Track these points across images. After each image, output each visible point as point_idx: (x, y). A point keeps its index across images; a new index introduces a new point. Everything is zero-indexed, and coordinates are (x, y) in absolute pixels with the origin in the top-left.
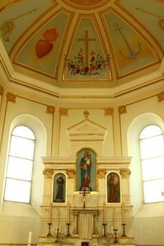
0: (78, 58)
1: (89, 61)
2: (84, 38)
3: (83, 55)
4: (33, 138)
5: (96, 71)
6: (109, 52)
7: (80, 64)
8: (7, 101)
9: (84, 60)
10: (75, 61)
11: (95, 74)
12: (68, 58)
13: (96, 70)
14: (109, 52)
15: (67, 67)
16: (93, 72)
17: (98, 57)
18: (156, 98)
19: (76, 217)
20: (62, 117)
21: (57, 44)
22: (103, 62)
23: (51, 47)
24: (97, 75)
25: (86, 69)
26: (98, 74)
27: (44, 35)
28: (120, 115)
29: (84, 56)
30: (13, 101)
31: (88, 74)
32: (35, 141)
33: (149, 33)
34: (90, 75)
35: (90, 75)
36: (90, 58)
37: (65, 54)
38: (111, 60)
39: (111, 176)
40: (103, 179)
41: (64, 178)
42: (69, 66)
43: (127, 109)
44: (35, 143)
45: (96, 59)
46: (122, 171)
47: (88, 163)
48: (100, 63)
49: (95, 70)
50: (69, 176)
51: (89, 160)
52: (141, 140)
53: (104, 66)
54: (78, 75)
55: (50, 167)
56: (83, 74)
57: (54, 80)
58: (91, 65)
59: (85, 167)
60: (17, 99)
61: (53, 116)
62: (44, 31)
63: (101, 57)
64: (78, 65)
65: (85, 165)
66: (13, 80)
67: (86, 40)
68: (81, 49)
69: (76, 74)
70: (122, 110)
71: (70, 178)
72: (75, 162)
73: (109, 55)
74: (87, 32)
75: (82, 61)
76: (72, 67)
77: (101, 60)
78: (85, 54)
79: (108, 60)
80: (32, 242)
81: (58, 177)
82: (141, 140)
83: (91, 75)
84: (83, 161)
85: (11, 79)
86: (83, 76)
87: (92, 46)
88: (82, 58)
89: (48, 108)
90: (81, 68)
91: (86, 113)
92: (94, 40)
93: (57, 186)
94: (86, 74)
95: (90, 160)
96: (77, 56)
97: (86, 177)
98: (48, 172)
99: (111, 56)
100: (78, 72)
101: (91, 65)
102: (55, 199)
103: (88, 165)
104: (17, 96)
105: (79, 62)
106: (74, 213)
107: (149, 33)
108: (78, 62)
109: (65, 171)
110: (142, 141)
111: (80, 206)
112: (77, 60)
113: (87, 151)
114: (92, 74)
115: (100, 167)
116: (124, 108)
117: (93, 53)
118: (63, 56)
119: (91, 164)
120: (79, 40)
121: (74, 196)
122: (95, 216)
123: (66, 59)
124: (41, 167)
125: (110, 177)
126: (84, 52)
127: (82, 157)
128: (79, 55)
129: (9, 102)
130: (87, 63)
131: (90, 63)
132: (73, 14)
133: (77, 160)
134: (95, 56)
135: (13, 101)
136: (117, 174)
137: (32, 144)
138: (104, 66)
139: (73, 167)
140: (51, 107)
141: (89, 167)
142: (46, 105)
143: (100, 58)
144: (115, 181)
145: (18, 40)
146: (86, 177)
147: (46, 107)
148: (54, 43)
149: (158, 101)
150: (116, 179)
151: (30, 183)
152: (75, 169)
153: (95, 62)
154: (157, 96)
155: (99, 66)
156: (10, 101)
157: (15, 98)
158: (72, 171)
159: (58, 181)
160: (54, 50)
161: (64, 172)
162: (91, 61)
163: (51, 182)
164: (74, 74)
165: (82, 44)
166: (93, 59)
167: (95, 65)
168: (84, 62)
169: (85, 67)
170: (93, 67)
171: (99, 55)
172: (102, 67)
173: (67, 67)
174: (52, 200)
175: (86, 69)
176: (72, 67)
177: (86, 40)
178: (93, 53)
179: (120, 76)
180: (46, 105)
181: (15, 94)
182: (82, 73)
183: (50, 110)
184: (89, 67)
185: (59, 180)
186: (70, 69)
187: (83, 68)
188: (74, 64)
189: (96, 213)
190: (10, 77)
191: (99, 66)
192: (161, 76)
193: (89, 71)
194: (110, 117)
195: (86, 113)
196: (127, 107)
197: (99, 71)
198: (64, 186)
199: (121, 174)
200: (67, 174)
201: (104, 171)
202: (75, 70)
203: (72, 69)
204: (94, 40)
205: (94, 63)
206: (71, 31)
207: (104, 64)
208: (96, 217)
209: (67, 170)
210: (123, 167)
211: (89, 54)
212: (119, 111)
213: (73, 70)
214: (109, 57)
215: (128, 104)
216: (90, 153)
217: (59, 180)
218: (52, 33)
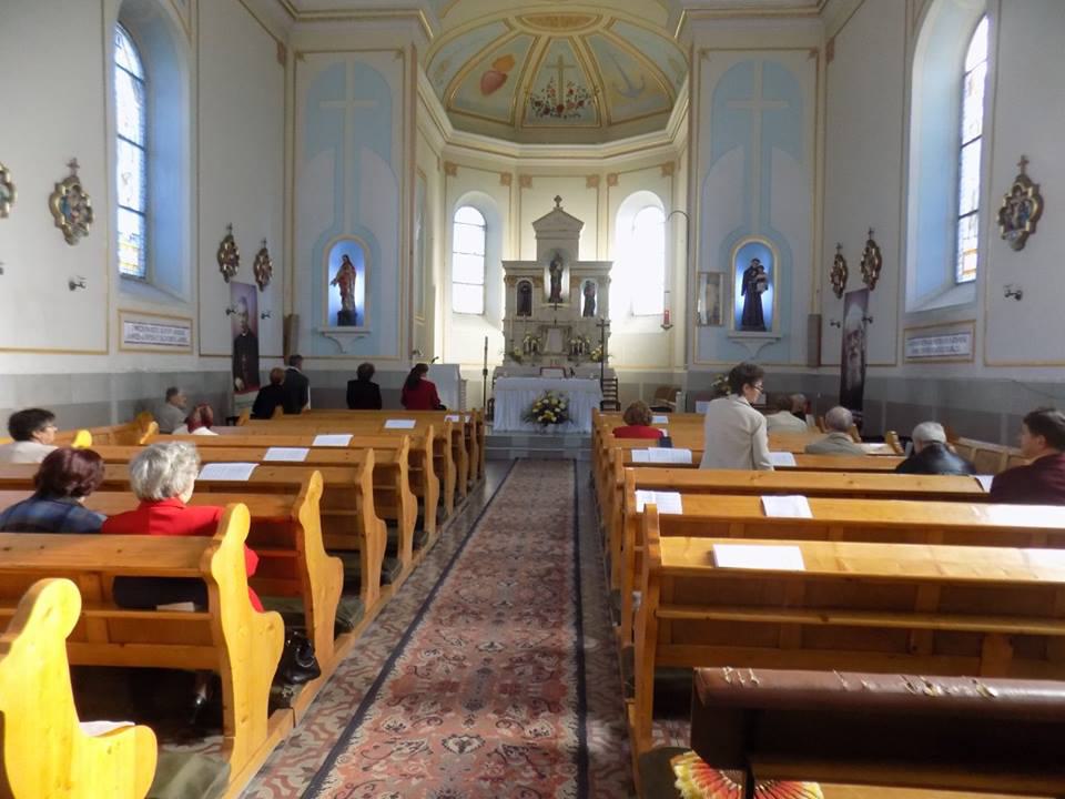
1: (564, 95)
4: (482, 223)
9: (557, 93)
20: (523, 190)
22: (587, 96)
23: (504, 78)
27: (494, 65)
29: (557, 88)
32: (486, 227)
36: (566, 91)
38: (600, 94)
43: (619, 180)
45: (575, 93)
62: (494, 60)
63: (584, 90)
70: (613, 179)
74: (561, 59)
75: (554, 95)
80: (91, 617)
88: (553, 91)
90: (551, 106)
92: (572, 67)
100: (547, 111)
104: (458, 165)
111: (549, 320)
117: (570, 84)
118: (523, 87)
121: (543, 308)
128: (549, 86)
130: (561, 97)
131: (565, 99)
132: (537, 38)
137: (481, 234)
147: (499, 176)
148: (510, 74)
152: (457, 702)
153: (573, 97)
160: (508, 80)
166: (571, 92)
167: (573, 101)
177: (561, 66)
183: (506, 178)
184: (565, 104)
189: (568, 330)
194: (594, 190)
202: (542, 110)
203: (537, 108)
204: (572, 67)
206: (536, 55)
211: (565, 84)
212: (608, 180)
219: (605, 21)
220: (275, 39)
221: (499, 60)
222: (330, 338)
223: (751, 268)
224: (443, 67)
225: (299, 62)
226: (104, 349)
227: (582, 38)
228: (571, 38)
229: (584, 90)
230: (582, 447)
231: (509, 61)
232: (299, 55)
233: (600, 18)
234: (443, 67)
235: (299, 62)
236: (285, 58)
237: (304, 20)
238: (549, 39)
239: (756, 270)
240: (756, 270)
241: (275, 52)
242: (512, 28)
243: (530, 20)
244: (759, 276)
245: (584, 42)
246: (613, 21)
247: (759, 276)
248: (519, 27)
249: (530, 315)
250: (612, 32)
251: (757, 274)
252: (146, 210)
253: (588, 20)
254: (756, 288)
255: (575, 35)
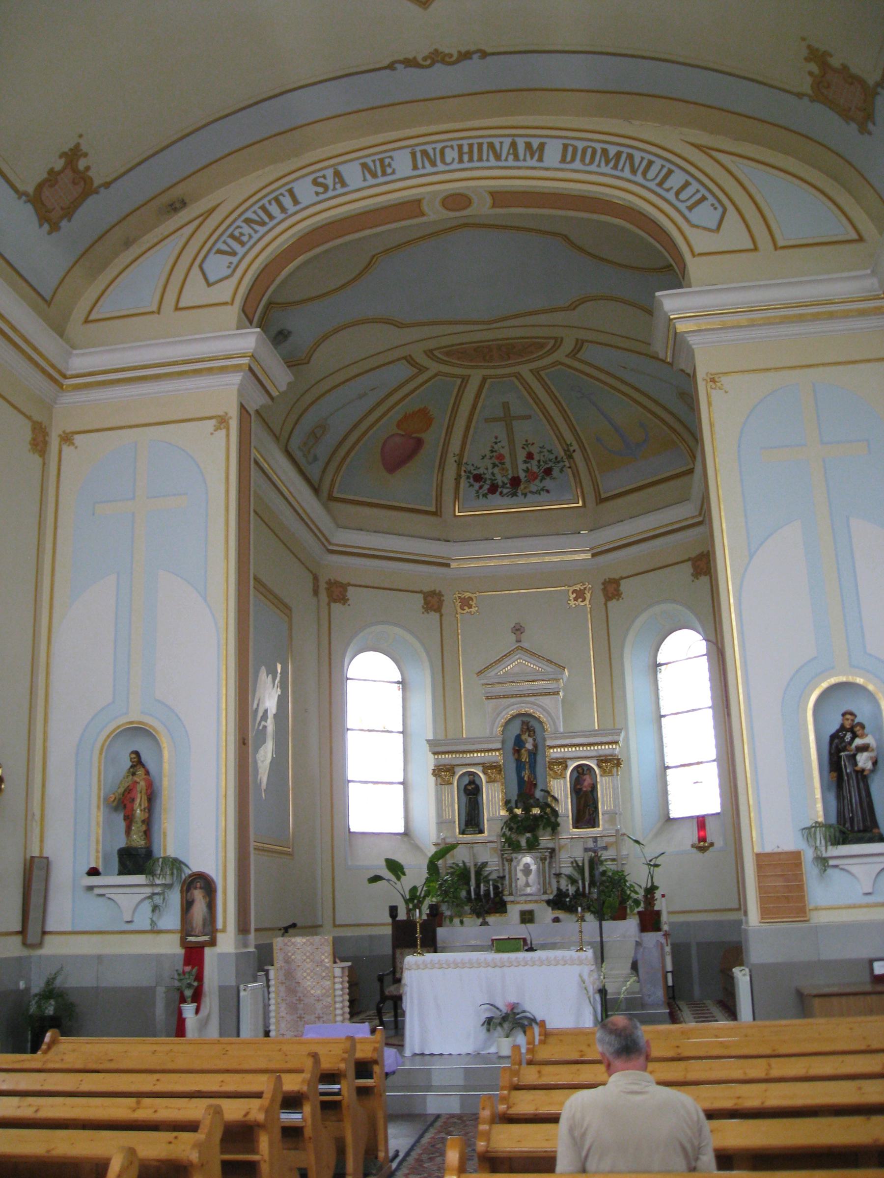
0: (491, 458)
2: (502, 415)
3: (502, 451)
5: (541, 485)
6: (569, 437)
7: (496, 470)
8: (329, 604)
9: (507, 460)
10: (484, 467)
11: (538, 492)
12: (464, 461)
13: (541, 481)
14: (569, 437)
15: (463, 483)
16: (533, 488)
17: (541, 452)
18: (688, 568)
19: (506, 863)
21: (432, 437)
22: (557, 460)
23: (419, 443)
24: (544, 494)
25: (515, 482)
26: (548, 491)
28: (606, 604)
29: (505, 452)
30: (342, 599)
31: (519, 494)
32: (403, 683)
33: (671, 413)
34: (525, 495)
35: (525, 495)
36: (521, 455)
37: (457, 452)
38: (578, 456)
39: (578, 772)
40: (428, 1100)
41: (478, 782)
42: (468, 478)
44: (404, 691)
45: (537, 457)
46: (602, 761)
47: (529, 746)
48: (550, 465)
49: (537, 482)
50: (490, 777)
51: (530, 740)
52: (660, 665)
53: (561, 471)
54: (495, 498)
55: (446, 759)
56: (507, 495)
57: (432, 519)
58: (527, 471)
59: (525, 757)
60: (351, 592)
61: (441, 616)
63: (550, 452)
64: (493, 474)
65: (523, 751)
66: (335, 548)
67: (507, 418)
68: (496, 438)
69: (490, 496)
71: (490, 781)
72: (499, 746)
73: (571, 445)
74: (506, 406)
75: (503, 464)
76: (478, 478)
77: (552, 457)
78: (507, 448)
79: (570, 457)
81: (466, 780)
82: (660, 665)
83: (529, 495)
84: (519, 743)
85: (330, 547)
86: (507, 500)
87: (523, 431)
88: (501, 457)
89: (425, 599)
90: (500, 479)
91: (518, 630)
93: (464, 799)
94: (514, 494)
95: (534, 740)
96: (488, 454)
97: (526, 779)
98: (442, 772)
99: (575, 446)
100: (493, 489)
101: (527, 471)
102: (463, 827)
103: (529, 751)
104: (349, 584)
105: (494, 465)
106: (503, 855)
107: (671, 413)
108: (490, 466)
109: (481, 768)
110: (663, 668)
112: (488, 463)
113: (525, 719)
114: (531, 492)
115: (555, 753)
116: (614, 586)
117: (527, 444)
119: (536, 746)
120: (487, 420)
122: (545, 859)
123: (459, 464)
124: (426, 761)
125: (575, 774)
126: (505, 443)
127: (518, 732)
128: (492, 451)
129: (333, 605)
130: (515, 466)
132: (465, 380)
133: (503, 742)
134: (534, 450)
135: (342, 599)
136: (590, 768)
137: (396, 693)
138: (561, 471)
139: (496, 757)
140: (433, 593)
141: (533, 754)
142: (421, 592)
143: (546, 453)
144: (586, 784)
145: (341, 443)
146: (526, 779)
147: (421, 596)
148: (426, 436)
149: (692, 575)
150: (588, 781)
151: (401, 787)
153: (534, 463)
154: (690, 563)
155: (548, 472)
156: (335, 601)
157: (346, 591)
158: (495, 767)
159: (465, 789)
161: (478, 771)
162: (525, 462)
163: (453, 794)
164: (485, 496)
165: (499, 430)
166: (530, 456)
167: (535, 469)
168: (508, 465)
169: (510, 477)
170: (532, 476)
171: (543, 447)
172: (555, 472)
173: (463, 483)
174: (457, 830)
175: (515, 482)
176: (478, 478)
178: (527, 444)
179: (603, 496)
180: (421, 592)
181: (345, 581)
182: (505, 491)
184: (522, 475)
185: (470, 788)
186: (471, 485)
187: (506, 481)
188: (481, 471)
190: (330, 543)
191: (548, 472)
192: (697, 513)
193: (522, 486)
195: (518, 630)
196: (622, 582)
197: (548, 483)
198: (479, 798)
199: (599, 766)
200: (485, 773)
201: (563, 762)
202: (486, 487)
203: (477, 485)
204: (528, 417)
205: (533, 466)
207: (561, 464)
208: (547, 862)
209: (482, 764)
210: (605, 749)
213: (481, 487)
214: (572, 449)
215: (624, 575)
216: (533, 723)
217: (470, 788)
218: (424, 417)
219: (568, 346)
220: (29, 418)
221: (406, 418)
222: (109, 898)
223: (842, 728)
224: (316, 435)
225: (65, 448)
226: (337, 923)
227: (536, 373)
228: (518, 376)
229: (550, 452)
230: (465, 1088)
231: (424, 417)
232: (67, 438)
233: (558, 342)
234: (316, 435)
235: (65, 448)
236: (46, 443)
237: (77, 387)
238: (484, 380)
239: (852, 730)
240: (852, 730)
241: (29, 436)
242: (422, 369)
243: (447, 354)
244: (858, 742)
245: (540, 379)
246: (580, 344)
247: (858, 742)
248: (434, 367)
249: (481, 832)
250: (582, 361)
251: (855, 736)
252: (403, 678)
253: (542, 346)
254: (856, 764)
255: (524, 370)
